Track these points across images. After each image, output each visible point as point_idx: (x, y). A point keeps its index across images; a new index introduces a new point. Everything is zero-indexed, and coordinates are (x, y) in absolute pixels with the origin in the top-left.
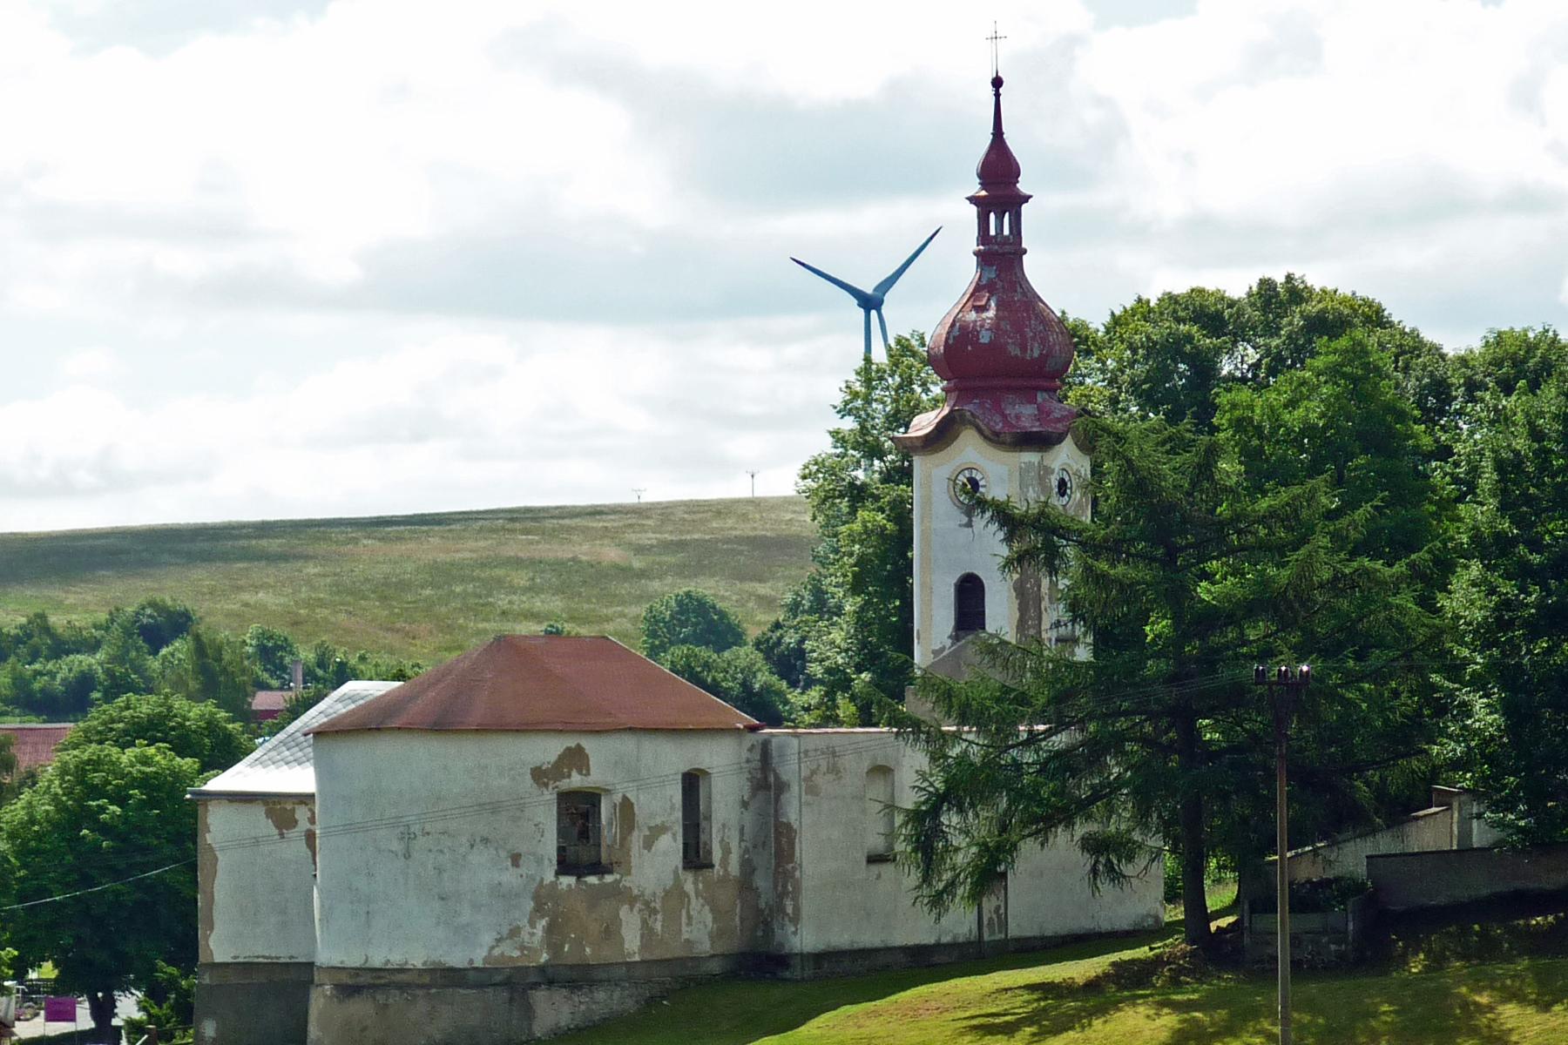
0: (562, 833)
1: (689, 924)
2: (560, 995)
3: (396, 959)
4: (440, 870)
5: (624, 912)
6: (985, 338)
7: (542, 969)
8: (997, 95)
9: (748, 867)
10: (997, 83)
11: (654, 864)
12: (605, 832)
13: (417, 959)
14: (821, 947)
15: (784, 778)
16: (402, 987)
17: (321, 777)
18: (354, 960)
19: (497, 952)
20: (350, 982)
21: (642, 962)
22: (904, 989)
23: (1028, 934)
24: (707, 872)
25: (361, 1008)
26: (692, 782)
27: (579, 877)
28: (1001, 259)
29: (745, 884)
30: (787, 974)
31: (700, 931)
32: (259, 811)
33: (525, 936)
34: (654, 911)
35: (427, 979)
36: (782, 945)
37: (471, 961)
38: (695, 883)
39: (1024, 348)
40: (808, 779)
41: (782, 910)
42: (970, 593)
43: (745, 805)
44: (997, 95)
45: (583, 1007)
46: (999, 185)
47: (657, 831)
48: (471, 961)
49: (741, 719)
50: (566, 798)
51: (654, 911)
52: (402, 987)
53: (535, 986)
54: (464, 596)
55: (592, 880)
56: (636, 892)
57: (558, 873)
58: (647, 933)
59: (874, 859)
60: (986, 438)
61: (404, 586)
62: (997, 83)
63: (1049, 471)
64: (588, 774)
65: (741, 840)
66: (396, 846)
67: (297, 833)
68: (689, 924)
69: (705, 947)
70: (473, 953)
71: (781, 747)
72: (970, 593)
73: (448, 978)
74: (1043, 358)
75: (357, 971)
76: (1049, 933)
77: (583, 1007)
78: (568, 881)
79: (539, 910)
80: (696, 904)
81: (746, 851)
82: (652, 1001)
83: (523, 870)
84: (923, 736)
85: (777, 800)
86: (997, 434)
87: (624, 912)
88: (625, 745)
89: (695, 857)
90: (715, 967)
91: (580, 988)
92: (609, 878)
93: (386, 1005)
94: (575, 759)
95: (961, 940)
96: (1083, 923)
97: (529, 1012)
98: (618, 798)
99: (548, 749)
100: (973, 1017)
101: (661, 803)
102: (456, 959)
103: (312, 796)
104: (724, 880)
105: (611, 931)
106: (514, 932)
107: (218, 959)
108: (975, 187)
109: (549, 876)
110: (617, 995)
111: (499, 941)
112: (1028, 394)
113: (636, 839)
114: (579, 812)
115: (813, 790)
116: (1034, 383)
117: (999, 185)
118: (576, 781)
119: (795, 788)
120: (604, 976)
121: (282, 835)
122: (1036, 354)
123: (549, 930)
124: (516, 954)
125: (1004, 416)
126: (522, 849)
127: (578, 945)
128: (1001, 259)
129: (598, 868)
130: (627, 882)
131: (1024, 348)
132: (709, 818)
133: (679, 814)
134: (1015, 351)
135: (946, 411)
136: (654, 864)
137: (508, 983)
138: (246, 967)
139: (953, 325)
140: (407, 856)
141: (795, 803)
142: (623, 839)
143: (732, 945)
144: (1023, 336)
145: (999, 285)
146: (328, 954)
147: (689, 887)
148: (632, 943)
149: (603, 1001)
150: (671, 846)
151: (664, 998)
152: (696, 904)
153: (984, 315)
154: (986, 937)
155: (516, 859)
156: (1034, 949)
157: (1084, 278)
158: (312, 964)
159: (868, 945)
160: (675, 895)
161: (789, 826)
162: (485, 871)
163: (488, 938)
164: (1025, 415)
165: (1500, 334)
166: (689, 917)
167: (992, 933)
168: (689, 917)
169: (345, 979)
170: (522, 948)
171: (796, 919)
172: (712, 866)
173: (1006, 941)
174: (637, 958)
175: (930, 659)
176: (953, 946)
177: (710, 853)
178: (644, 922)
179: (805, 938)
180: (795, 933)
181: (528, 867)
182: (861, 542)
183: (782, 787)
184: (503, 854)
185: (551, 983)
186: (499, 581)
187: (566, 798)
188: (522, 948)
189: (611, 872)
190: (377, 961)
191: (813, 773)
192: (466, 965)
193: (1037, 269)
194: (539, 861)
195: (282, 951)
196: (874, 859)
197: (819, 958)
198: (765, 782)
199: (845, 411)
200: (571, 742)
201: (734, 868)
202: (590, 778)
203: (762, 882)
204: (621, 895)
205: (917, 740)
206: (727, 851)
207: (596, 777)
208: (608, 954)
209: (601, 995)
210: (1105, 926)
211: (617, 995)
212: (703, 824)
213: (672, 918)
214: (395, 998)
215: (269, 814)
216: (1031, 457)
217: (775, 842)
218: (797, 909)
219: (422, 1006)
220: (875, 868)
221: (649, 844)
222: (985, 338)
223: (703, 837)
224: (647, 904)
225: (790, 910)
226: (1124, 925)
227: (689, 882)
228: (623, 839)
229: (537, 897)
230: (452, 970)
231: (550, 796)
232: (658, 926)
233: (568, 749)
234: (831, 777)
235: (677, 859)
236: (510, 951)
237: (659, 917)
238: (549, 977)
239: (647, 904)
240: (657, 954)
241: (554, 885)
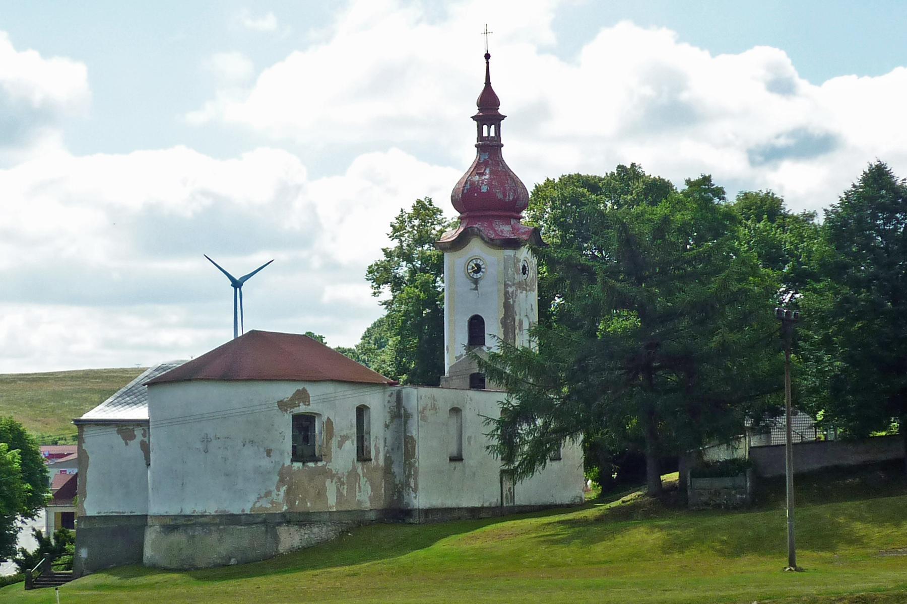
0: (294, 438)
1: (360, 491)
2: (293, 529)
3: (199, 509)
4: (225, 459)
5: (328, 482)
6: (484, 189)
7: (283, 515)
8: (488, 63)
9: (388, 461)
10: (487, 56)
11: (342, 457)
12: (317, 438)
13: (212, 509)
14: (428, 506)
15: (410, 411)
16: (203, 525)
17: (151, 411)
18: (174, 510)
19: (258, 505)
20: (172, 523)
21: (337, 511)
22: (473, 530)
23: (524, 504)
24: (368, 463)
25: (179, 538)
26: (361, 411)
27: (304, 463)
28: (490, 149)
29: (387, 470)
30: (411, 521)
31: (366, 497)
32: (113, 430)
33: (274, 495)
34: (342, 484)
35: (218, 521)
36: (408, 504)
37: (243, 510)
38: (363, 469)
39: (505, 195)
40: (422, 412)
41: (408, 485)
42: (476, 327)
43: (387, 426)
44: (488, 63)
45: (306, 536)
46: (488, 109)
47: (345, 438)
48: (243, 510)
49: (386, 380)
50: (297, 418)
51: (342, 484)
52: (203, 525)
53: (280, 524)
54: (70, 405)
55: (311, 464)
56: (334, 472)
57: (292, 461)
58: (339, 495)
59: (452, 459)
60: (486, 242)
61: (39, 401)
62: (487, 56)
63: (519, 261)
64: (309, 405)
65: (385, 446)
66: (199, 445)
67: (135, 444)
68: (360, 491)
69: (367, 505)
70: (244, 505)
71: (408, 395)
72: (476, 327)
73: (232, 520)
74: (515, 201)
75: (176, 517)
76: (533, 504)
77: (306, 536)
78: (298, 465)
79: (282, 481)
80: (363, 480)
81: (388, 452)
82: (342, 534)
83: (273, 459)
84: (504, 381)
85: (406, 423)
86: (492, 240)
87: (328, 482)
88: (328, 389)
89: (363, 455)
90: (372, 516)
91: (305, 525)
92: (320, 464)
93: (193, 536)
94: (302, 396)
95: (493, 505)
96: (547, 499)
97: (276, 539)
98: (324, 419)
99: (286, 391)
100: (542, 536)
101: (345, 423)
102: (235, 510)
103: (147, 421)
104: (376, 468)
105: (321, 494)
106: (268, 494)
107: (89, 514)
108: (475, 111)
109: (288, 462)
110: (324, 529)
111: (260, 498)
112: (507, 219)
113: (334, 443)
114: (304, 425)
115: (424, 418)
116: (508, 214)
117: (488, 109)
118: (302, 409)
119: (415, 417)
120: (318, 519)
121: (127, 444)
122: (511, 198)
123: (288, 492)
124: (269, 506)
125: (495, 231)
126: (273, 446)
127: (303, 500)
128: (490, 149)
129: (315, 459)
130: (330, 466)
131: (505, 195)
132: (369, 433)
133: (355, 430)
134: (500, 196)
135: (462, 229)
136: (342, 457)
137: (264, 522)
138: (106, 518)
139: (466, 183)
140: (206, 451)
141: (415, 426)
142: (327, 442)
143: (380, 504)
144: (504, 189)
145: (490, 162)
146: (154, 509)
147: (360, 471)
148: (332, 501)
149: (318, 533)
150: (350, 446)
151: (348, 532)
152: (363, 480)
153: (484, 177)
154: (505, 504)
155: (269, 453)
156: (530, 512)
157: (534, 160)
158: (145, 517)
159: (450, 506)
160: (353, 474)
161: (412, 437)
162: (251, 459)
163: (253, 498)
164: (505, 230)
165: (746, 194)
166: (360, 487)
167: (507, 502)
168: (360, 487)
169: (168, 522)
170: (272, 502)
171: (415, 490)
172: (371, 460)
173: (514, 507)
174: (335, 510)
175: (455, 361)
176: (489, 509)
177: (370, 452)
178: (338, 489)
179: (420, 501)
180: (415, 498)
181: (275, 457)
182: (407, 304)
183: (408, 416)
184: (262, 449)
185: (289, 522)
186: (86, 399)
187: (297, 418)
188: (272, 502)
189: (321, 461)
190: (188, 511)
191: (424, 409)
192: (240, 513)
193: (513, 153)
194: (282, 453)
195: (126, 509)
196: (452, 459)
197: (428, 512)
198: (399, 414)
199: (392, 237)
200: (299, 386)
201: (381, 462)
202: (310, 407)
203: (396, 469)
204: (327, 473)
205: (501, 382)
206: (377, 453)
207: (312, 408)
208: (319, 507)
209: (316, 530)
210: (558, 502)
211: (324, 529)
212: (366, 436)
213: (351, 489)
214: (198, 532)
215: (119, 432)
216: (510, 253)
217: (404, 446)
218: (416, 484)
219: (215, 536)
220: (453, 464)
221: (340, 446)
222: (484, 189)
223: (366, 443)
224: (339, 479)
225: (412, 485)
226: (567, 501)
227: (359, 466)
228: (327, 442)
229: (281, 474)
230: (233, 515)
231: (288, 418)
232: (345, 493)
233: (298, 390)
234: (432, 412)
235: (354, 455)
236: (266, 504)
237: (345, 487)
238: (287, 519)
239: (339, 479)
240: (344, 508)
241: (290, 467)
